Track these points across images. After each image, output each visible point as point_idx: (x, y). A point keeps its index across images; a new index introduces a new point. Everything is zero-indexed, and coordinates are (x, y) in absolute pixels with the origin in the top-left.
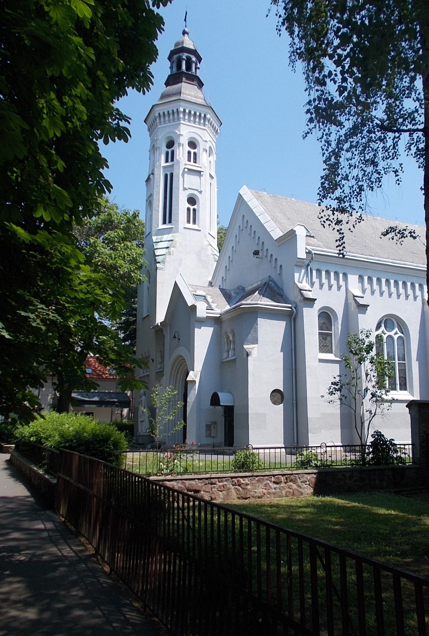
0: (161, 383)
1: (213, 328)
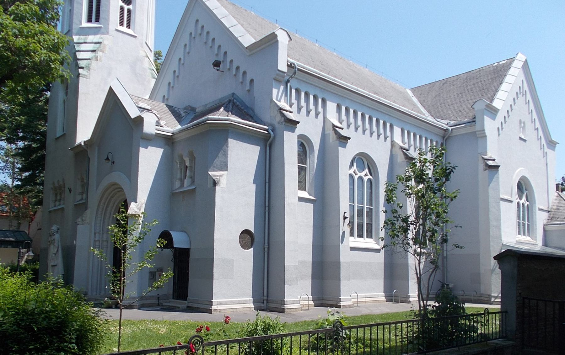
0: (84, 218)
1: (163, 149)
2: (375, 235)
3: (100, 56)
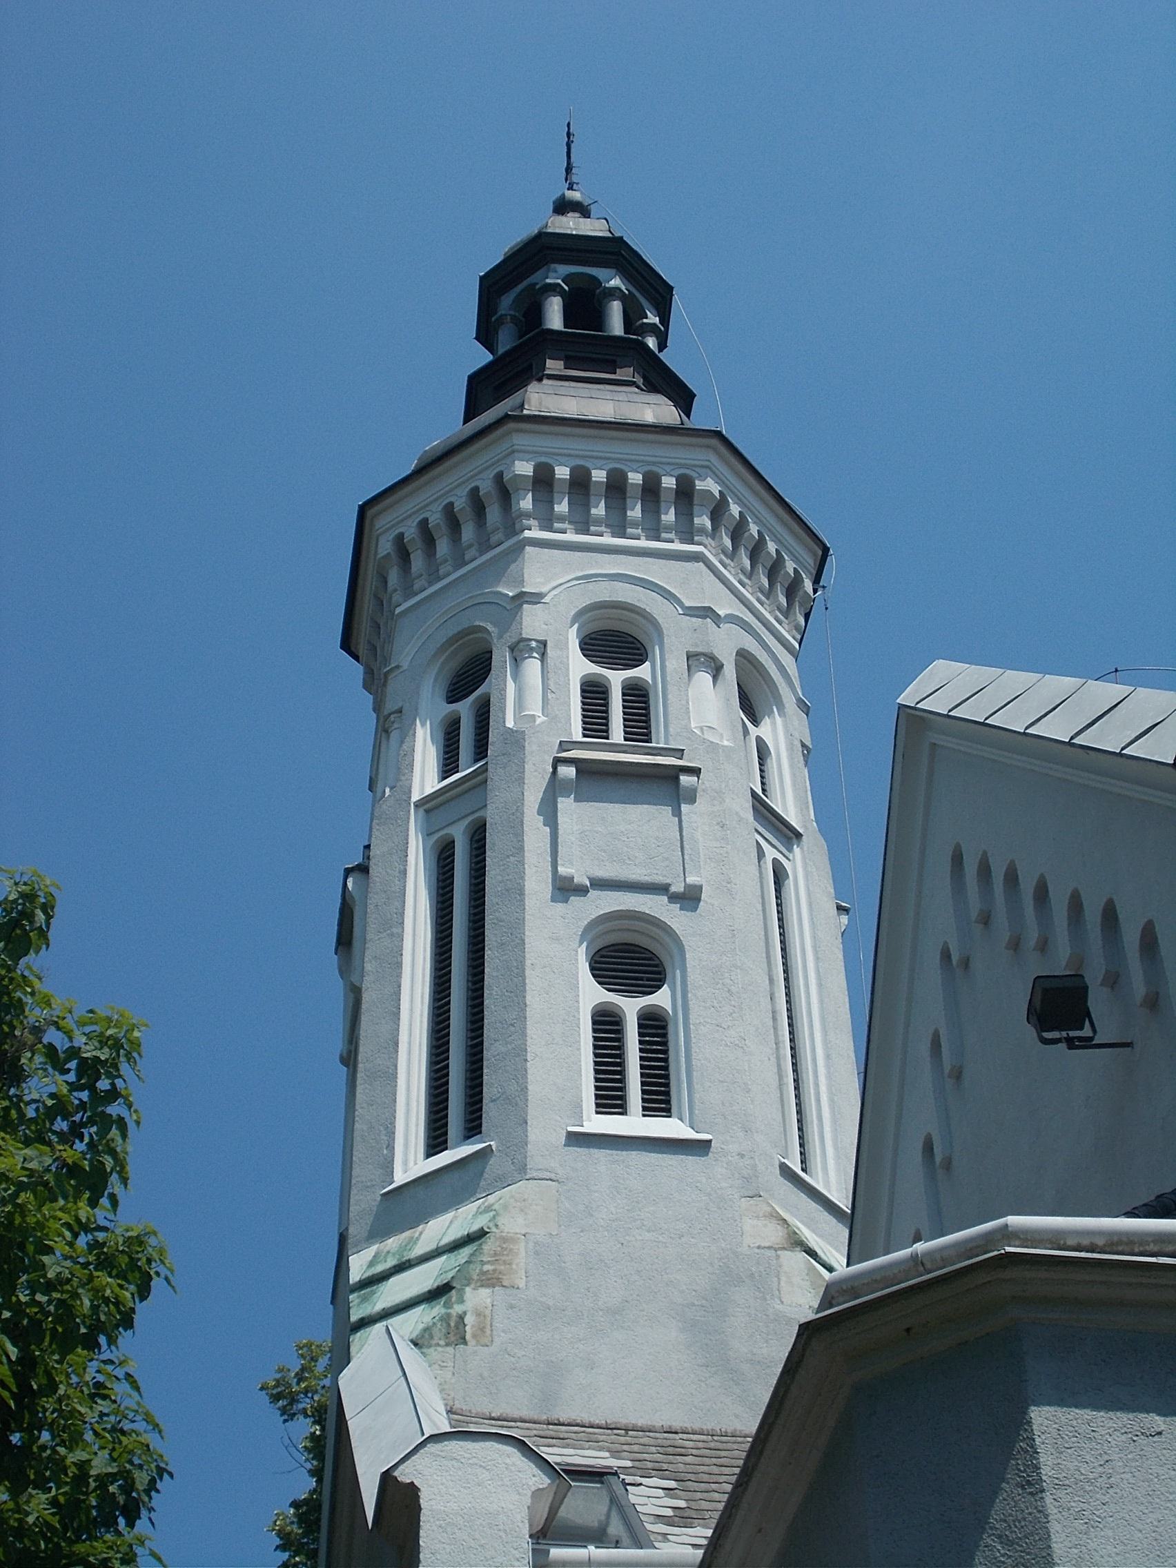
2: (415, 822)
3: (479, 1314)
